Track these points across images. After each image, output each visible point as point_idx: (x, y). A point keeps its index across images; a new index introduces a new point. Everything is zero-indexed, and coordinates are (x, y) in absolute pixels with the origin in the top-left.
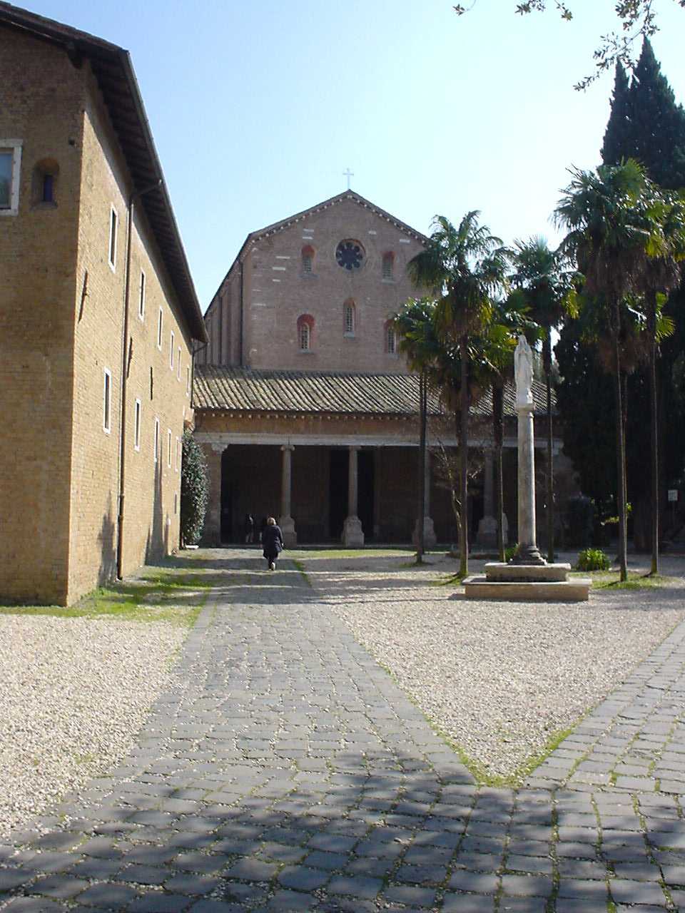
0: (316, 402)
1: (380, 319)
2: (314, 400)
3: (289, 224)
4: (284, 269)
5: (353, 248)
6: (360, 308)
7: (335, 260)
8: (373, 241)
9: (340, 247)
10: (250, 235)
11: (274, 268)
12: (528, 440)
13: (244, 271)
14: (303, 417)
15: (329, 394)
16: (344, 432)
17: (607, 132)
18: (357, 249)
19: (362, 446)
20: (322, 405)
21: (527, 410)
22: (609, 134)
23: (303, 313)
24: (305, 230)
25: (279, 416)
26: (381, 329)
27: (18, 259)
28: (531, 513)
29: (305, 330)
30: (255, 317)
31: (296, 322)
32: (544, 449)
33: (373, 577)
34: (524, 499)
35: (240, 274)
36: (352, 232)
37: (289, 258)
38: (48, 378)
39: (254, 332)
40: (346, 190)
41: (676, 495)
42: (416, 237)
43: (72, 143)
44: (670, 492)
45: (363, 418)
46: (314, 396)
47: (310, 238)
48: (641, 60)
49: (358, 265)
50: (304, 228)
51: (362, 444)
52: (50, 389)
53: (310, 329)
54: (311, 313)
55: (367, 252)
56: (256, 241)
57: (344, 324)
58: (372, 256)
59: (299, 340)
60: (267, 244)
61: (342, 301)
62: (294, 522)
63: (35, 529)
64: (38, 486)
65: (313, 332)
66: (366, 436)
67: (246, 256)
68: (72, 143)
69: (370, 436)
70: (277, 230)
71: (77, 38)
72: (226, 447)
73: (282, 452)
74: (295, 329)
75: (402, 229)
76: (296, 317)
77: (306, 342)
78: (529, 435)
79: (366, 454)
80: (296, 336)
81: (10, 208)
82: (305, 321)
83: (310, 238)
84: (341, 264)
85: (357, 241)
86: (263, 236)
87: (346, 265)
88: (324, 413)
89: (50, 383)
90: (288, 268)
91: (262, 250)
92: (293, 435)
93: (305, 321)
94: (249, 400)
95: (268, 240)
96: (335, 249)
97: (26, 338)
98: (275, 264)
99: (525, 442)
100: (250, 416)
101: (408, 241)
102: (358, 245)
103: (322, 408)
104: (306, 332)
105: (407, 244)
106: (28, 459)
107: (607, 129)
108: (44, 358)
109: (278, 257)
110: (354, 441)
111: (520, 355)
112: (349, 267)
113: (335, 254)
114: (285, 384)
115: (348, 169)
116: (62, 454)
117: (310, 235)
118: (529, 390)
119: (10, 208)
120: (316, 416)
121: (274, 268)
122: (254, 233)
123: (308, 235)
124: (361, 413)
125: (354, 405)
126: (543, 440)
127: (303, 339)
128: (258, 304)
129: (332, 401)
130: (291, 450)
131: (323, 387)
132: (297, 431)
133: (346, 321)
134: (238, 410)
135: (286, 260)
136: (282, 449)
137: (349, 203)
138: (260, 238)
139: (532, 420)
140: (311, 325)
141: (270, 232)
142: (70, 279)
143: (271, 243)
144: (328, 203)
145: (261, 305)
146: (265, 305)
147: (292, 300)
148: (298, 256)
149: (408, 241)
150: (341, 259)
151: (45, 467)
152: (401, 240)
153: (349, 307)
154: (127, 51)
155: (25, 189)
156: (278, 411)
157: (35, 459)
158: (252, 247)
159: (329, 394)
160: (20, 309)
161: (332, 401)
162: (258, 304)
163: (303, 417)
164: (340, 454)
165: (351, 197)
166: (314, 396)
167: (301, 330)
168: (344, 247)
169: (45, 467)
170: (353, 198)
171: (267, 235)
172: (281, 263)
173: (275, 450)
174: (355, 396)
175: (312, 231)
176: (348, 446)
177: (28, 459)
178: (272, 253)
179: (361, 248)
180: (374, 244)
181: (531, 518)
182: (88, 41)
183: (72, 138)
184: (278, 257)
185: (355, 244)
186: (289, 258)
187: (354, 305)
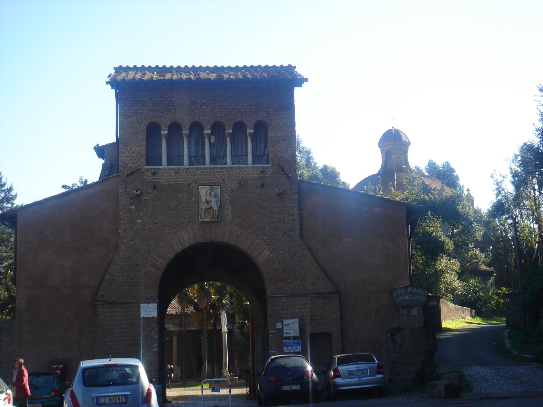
21: (225, 333)
41: (297, 326)
118: (226, 326)
139: (227, 336)
154: (112, 89)
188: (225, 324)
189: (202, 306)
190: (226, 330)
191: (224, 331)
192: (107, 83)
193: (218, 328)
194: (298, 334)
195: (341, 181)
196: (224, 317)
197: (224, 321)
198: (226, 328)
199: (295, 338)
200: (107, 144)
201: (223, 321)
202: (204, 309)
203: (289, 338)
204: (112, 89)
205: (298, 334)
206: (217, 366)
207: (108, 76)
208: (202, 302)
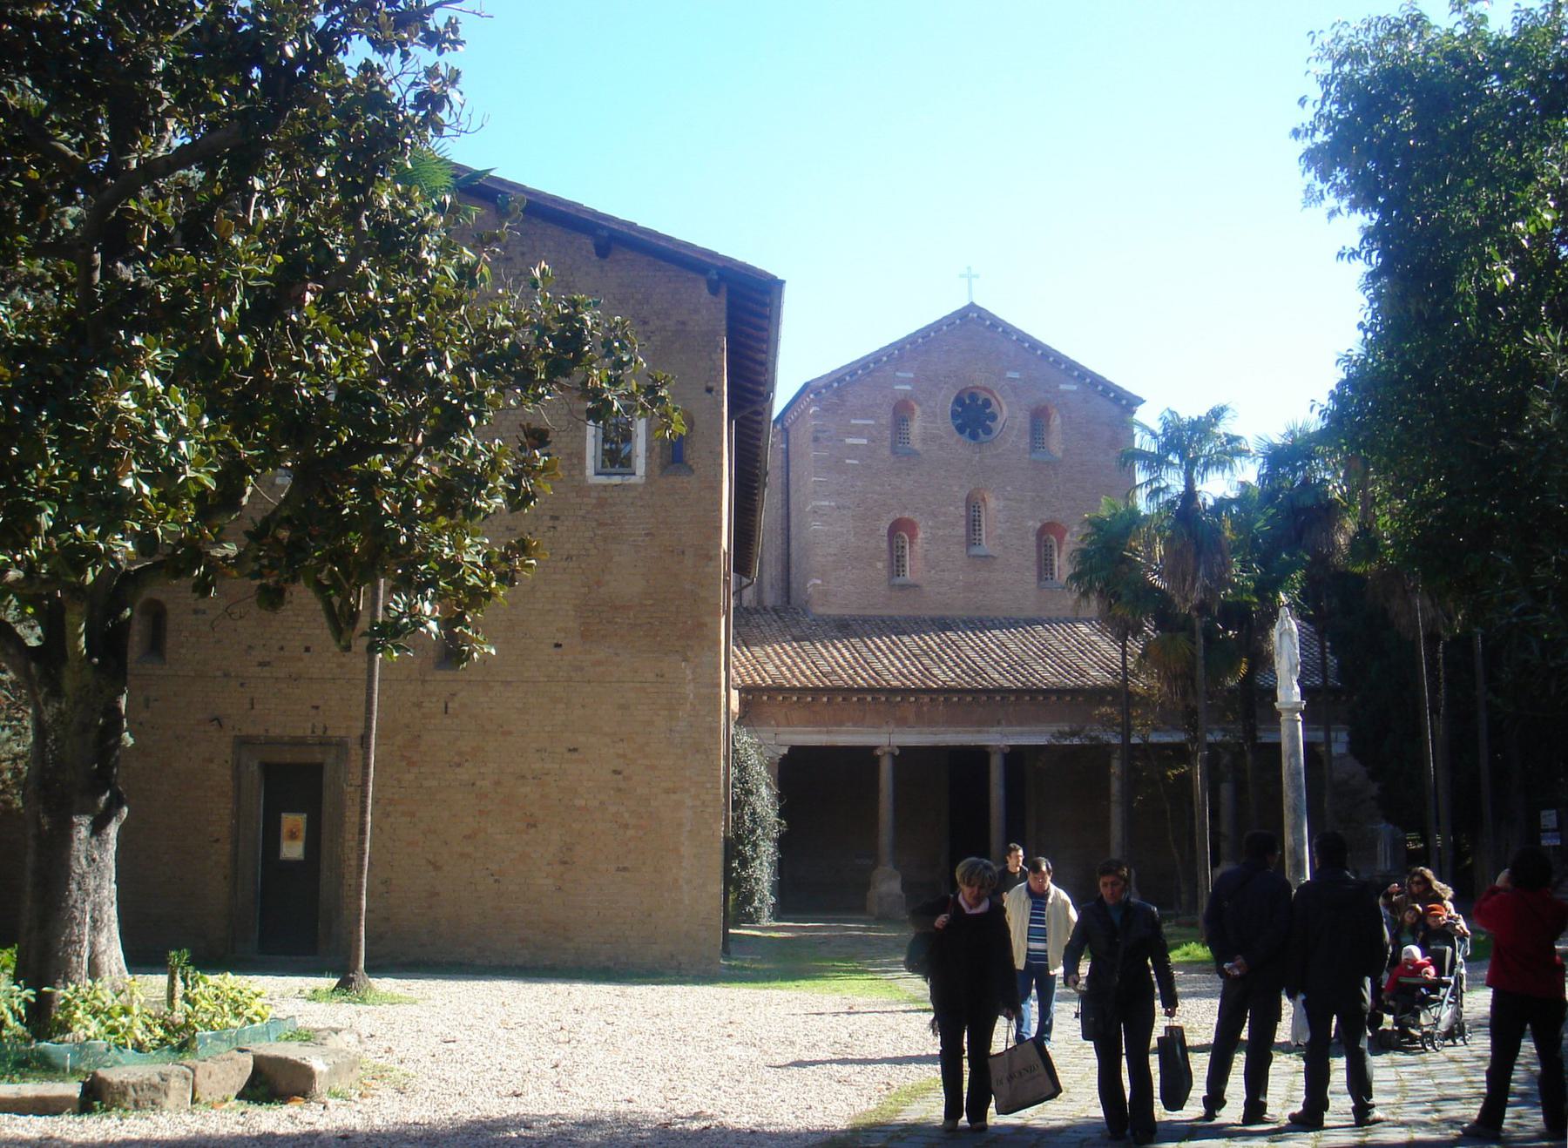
0: (930, 673)
1: (1031, 523)
2: (927, 670)
3: (872, 365)
4: (865, 441)
5: (980, 402)
6: (992, 504)
9: (959, 401)
10: (806, 385)
11: (849, 441)
12: (1294, 735)
13: (792, 440)
14: (912, 699)
15: (950, 657)
16: (982, 723)
18: (987, 403)
19: (1010, 746)
20: (942, 677)
21: (1293, 710)
23: (898, 516)
24: (898, 374)
27: (647, 539)
28: (1303, 853)
29: (901, 544)
30: (816, 526)
32: (1320, 744)
34: (1293, 833)
35: (784, 446)
36: (979, 377)
37: (872, 422)
38: (689, 689)
40: (966, 303)
41: (1554, 818)
43: (709, 390)
44: (1543, 813)
45: (1012, 698)
46: (926, 661)
47: (908, 387)
49: (988, 431)
50: (897, 370)
51: (1012, 743)
52: (691, 704)
53: (911, 543)
54: (911, 517)
55: (1005, 408)
56: (815, 395)
60: (835, 400)
61: (963, 494)
63: (676, 880)
64: (680, 825)
65: (916, 548)
66: (1018, 729)
67: (797, 418)
68: (709, 390)
69: (1026, 729)
70: (851, 376)
71: (720, 264)
72: (786, 752)
77: (903, 566)
78: (1298, 745)
79: (1015, 756)
81: (634, 474)
82: (900, 530)
83: (908, 387)
85: (985, 389)
86: (828, 386)
88: (946, 691)
89: (691, 696)
91: (827, 411)
92: (896, 730)
93: (900, 530)
94: (821, 672)
97: (659, 639)
98: (850, 434)
99: (1290, 756)
100: (825, 699)
101: (1075, 388)
102: (989, 396)
103: (944, 682)
104: (903, 547)
106: (667, 791)
108: (683, 664)
109: (853, 422)
110: (997, 738)
111: (1281, 635)
114: (876, 644)
115: (969, 268)
116: (709, 785)
117: (909, 384)
118: (1295, 683)
119: (634, 474)
120: (934, 696)
121: (849, 441)
122: (812, 381)
123: (903, 382)
124: (1009, 691)
125: (996, 676)
126: (1317, 730)
127: (898, 561)
128: (823, 503)
129: (957, 670)
131: (938, 645)
132: (902, 722)
133: (971, 528)
134: (805, 689)
136: (879, 752)
139: (1300, 724)
140: (913, 536)
141: (840, 380)
142: (712, 564)
145: (827, 503)
148: (886, 419)
149: (1075, 388)
150: (959, 421)
151: (689, 802)
152: (1062, 387)
153: (973, 508)
154: (782, 283)
155: (653, 450)
156: (871, 690)
157: (675, 793)
158: (808, 407)
159: (950, 657)
160: (651, 602)
161: (957, 670)
162: (823, 503)
163: (912, 699)
164: (976, 757)
165: (975, 315)
166: (926, 661)
168: (964, 401)
169: (689, 802)
172: (859, 432)
173: (865, 757)
174: (993, 659)
177: (667, 791)
179: (993, 401)
181: (1304, 860)
182: (736, 268)
183: (710, 384)
184: (853, 422)
185: (983, 395)
187: (984, 500)
188: (1291, 671)
189: (1186, 600)
190: (1299, 700)
191: (1286, 703)
192: (1217, 414)
193: (1266, 738)
194: (1555, 826)
195: (1149, 417)
196: (1286, 639)
197: (1285, 657)
198: (1297, 689)
199: (1554, 830)
200: (1104, 376)
201: (1280, 654)
202: (1194, 614)
203: (1547, 831)
204: (782, 283)
205: (1555, 826)
206: (978, 633)
207: (1173, 409)
208: (1185, 580)
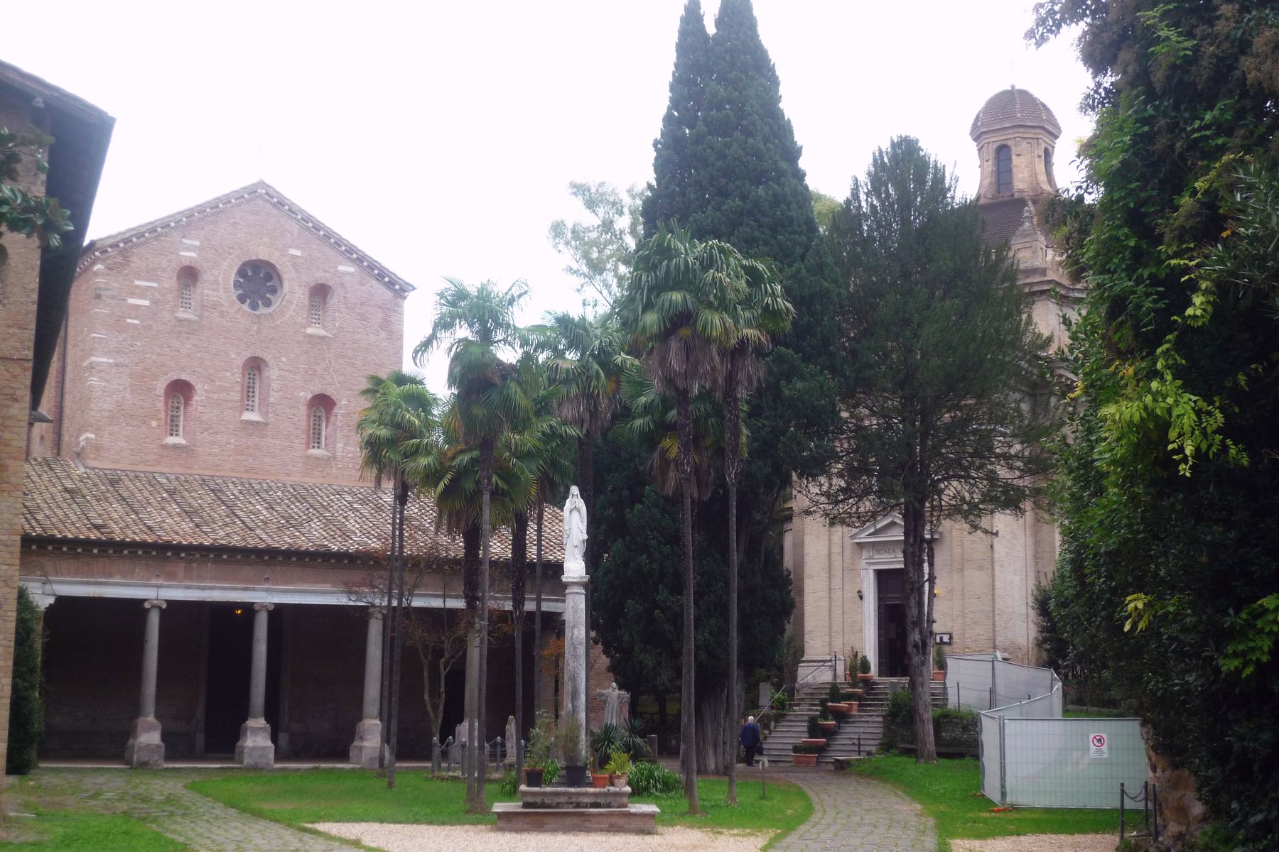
6: (272, 374)
7: (234, 294)
8: (295, 265)
11: (131, 301)
17: (676, 66)
19: (275, 604)
22: (688, 24)
24: (185, 241)
25: (144, 552)
26: (303, 410)
31: (162, 392)
33: (690, 716)
37: (155, 285)
39: (93, 406)
40: (255, 180)
42: (365, 264)
48: (592, 581)
50: (184, 237)
57: (242, 399)
58: (294, 290)
59: (166, 423)
60: (120, 259)
61: (240, 361)
62: (160, 726)
73: (147, 610)
74: (161, 405)
75: (343, 248)
76: (161, 386)
79: (279, 614)
80: (162, 415)
83: (193, 255)
84: (242, 299)
87: (248, 301)
90: (155, 302)
91: (111, 269)
95: (123, 253)
96: (233, 276)
98: (133, 295)
105: (351, 274)
107: (670, 94)
112: (254, 307)
113: (232, 283)
121: (131, 301)
127: (172, 421)
130: (160, 608)
135: (151, 287)
136: (147, 605)
137: (260, 202)
138: (109, 250)
141: (127, 241)
143: (127, 260)
144: (226, 200)
146: (111, 361)
147: (159, 355)
148: (171, 282)
165: (264, 191)
167: (170, 404)
170: (267, 194)
171: (122, 245)
172: (142, 293)
173: (135, 608)
175: (197, 243)
176: (253, 603)
178: (127, 275)
180: (297, 272)
184: (137, 283)
186: (155, 285)
